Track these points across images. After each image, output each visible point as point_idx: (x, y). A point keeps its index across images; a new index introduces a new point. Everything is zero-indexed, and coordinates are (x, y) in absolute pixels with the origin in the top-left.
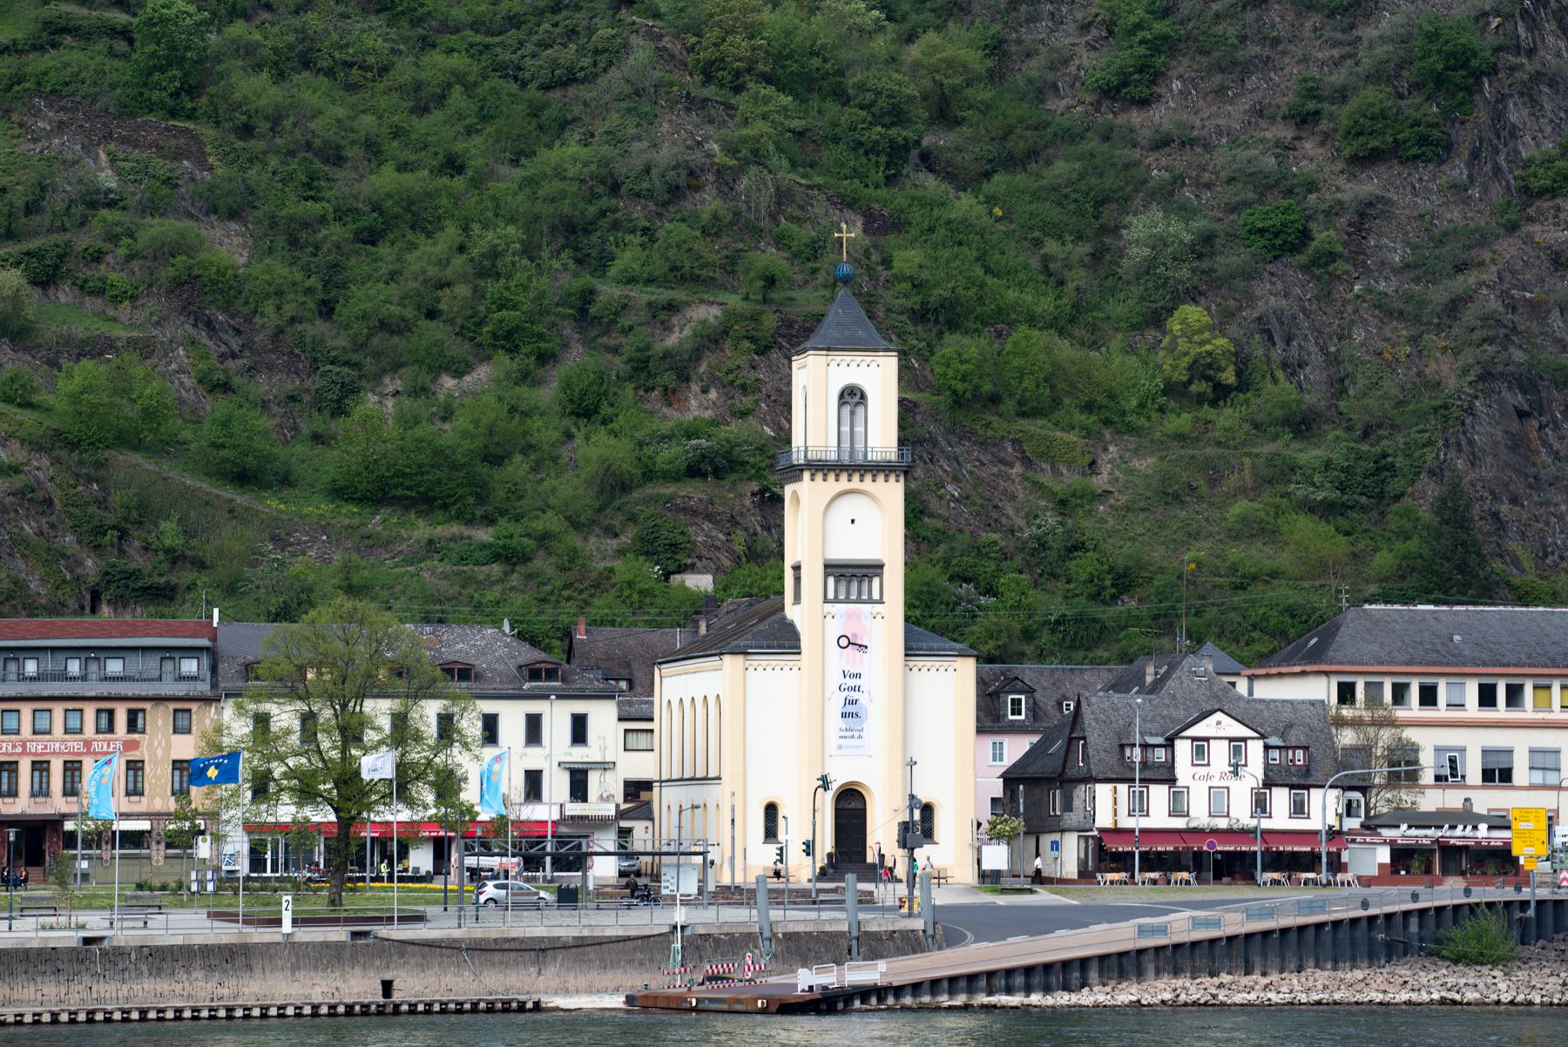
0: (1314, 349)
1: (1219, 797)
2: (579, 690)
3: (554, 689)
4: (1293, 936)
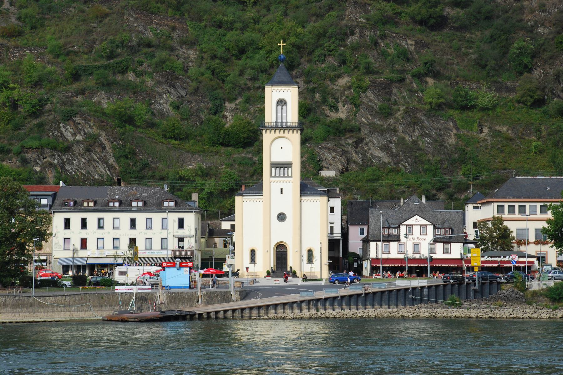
1: (416, 246)
4: (378, 296)
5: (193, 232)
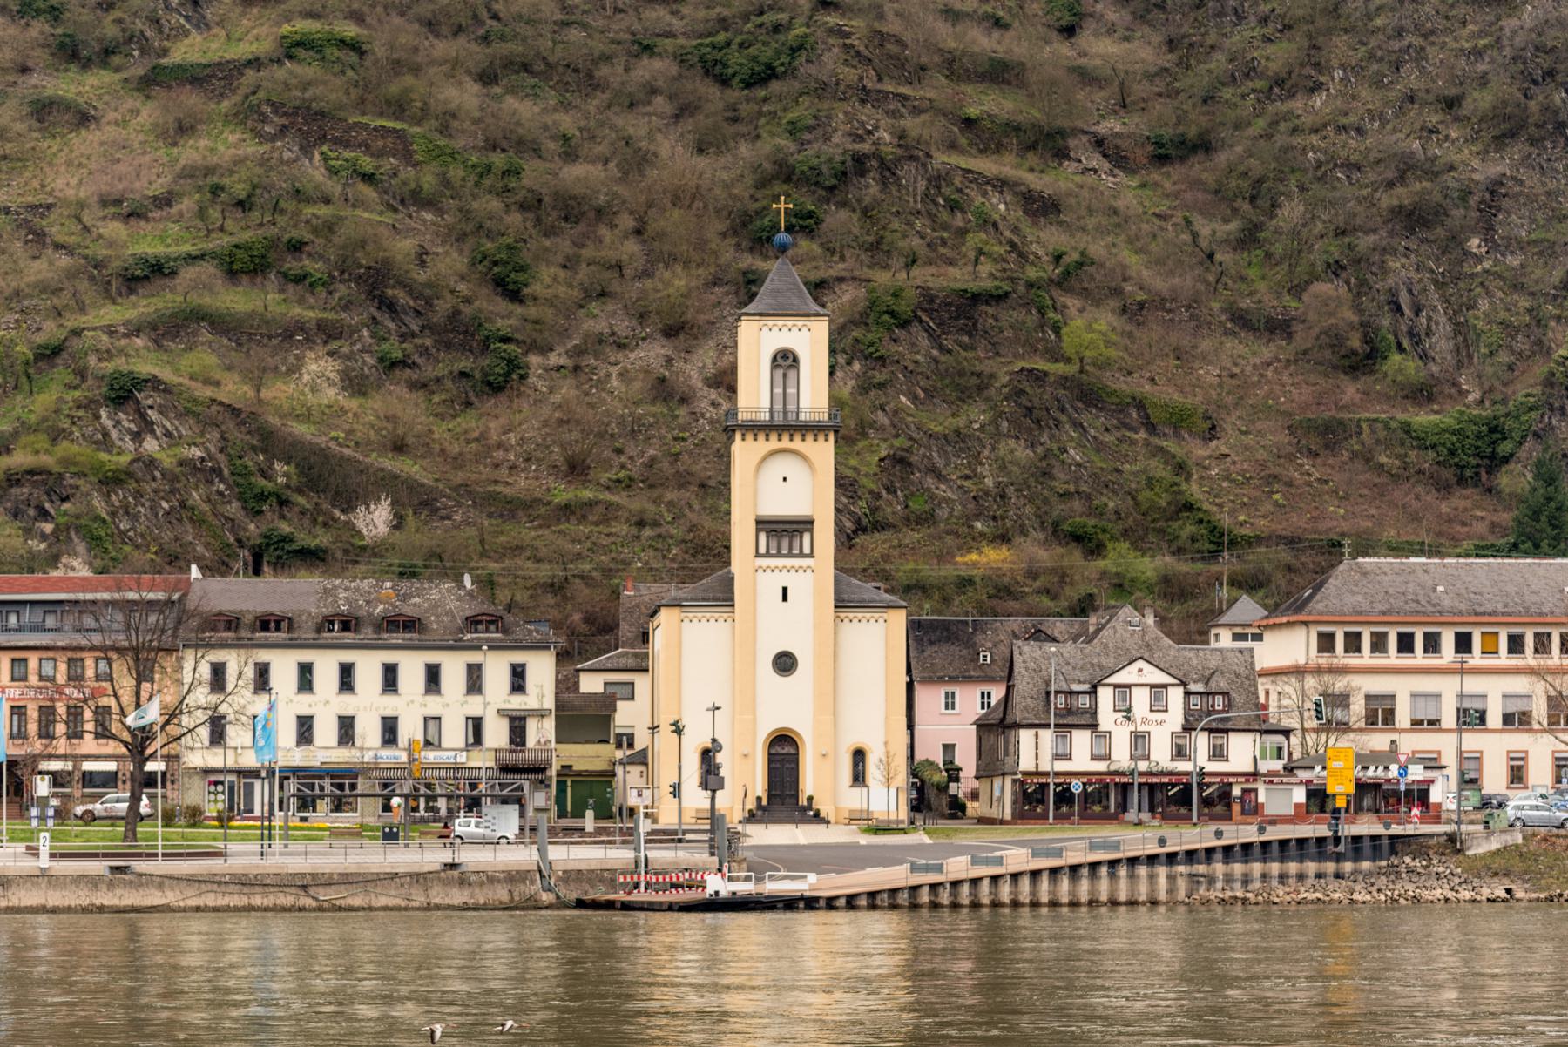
0: (1443, 319)
1: (1140, 740)
3: (487, 640)
5: (549, 703)
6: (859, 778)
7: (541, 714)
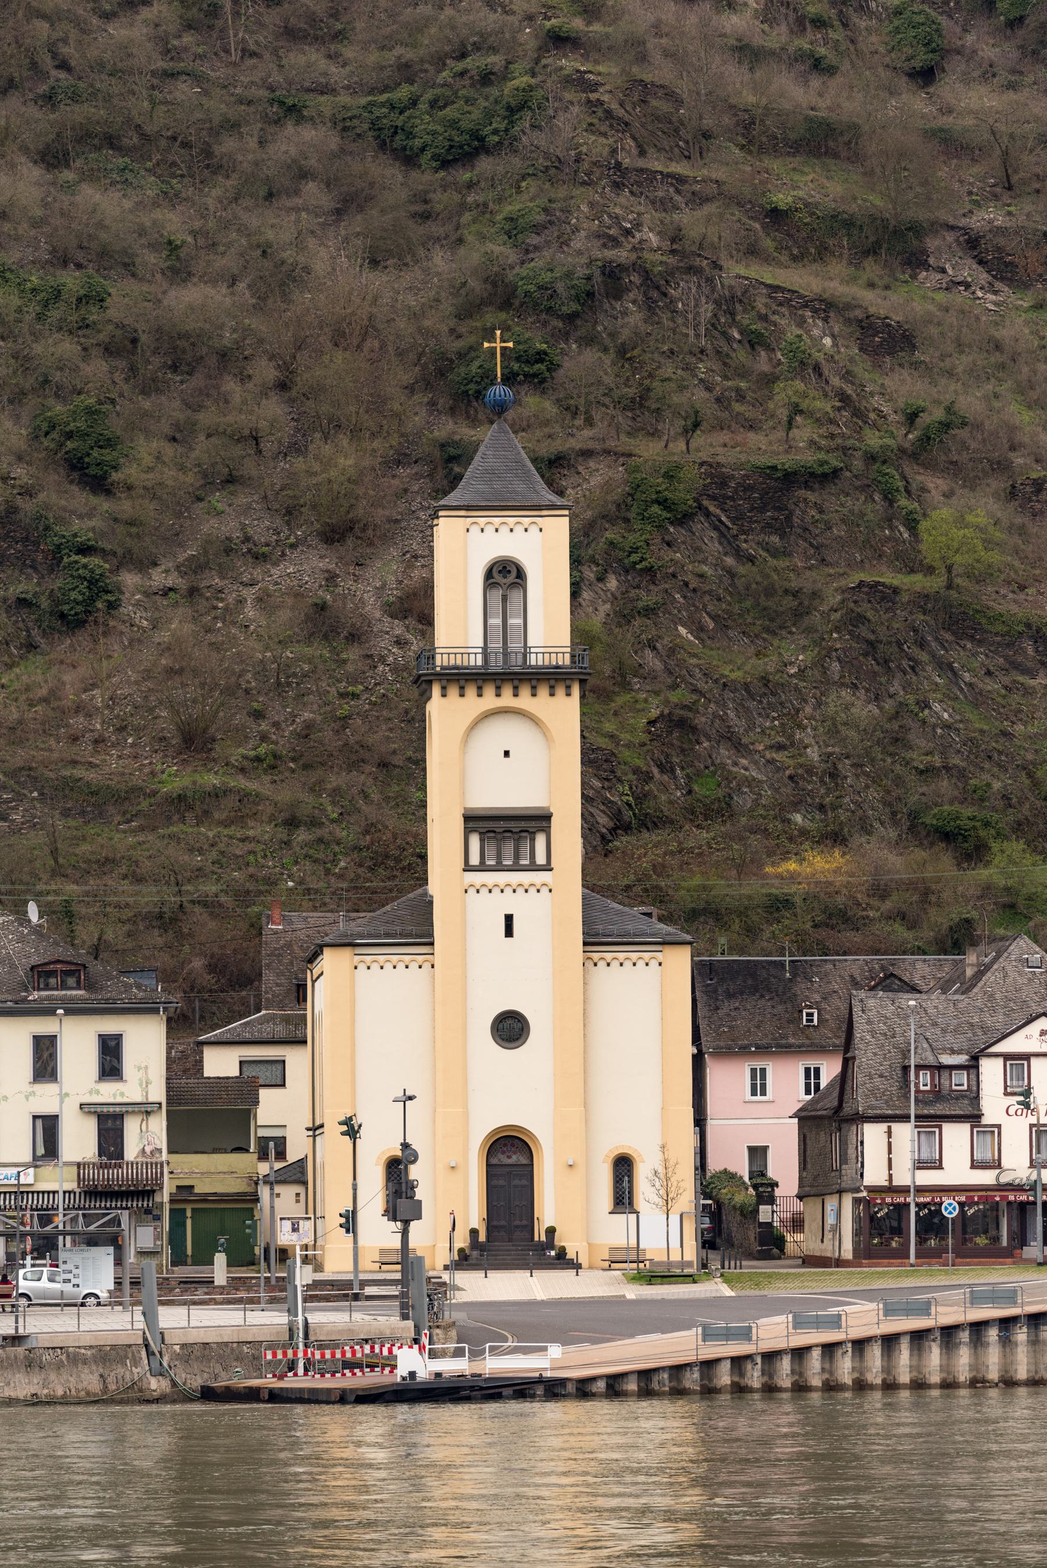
2: (107, 1001)
3: (63, 1000)
6: (623, 1199)
7: (146, 1110)
